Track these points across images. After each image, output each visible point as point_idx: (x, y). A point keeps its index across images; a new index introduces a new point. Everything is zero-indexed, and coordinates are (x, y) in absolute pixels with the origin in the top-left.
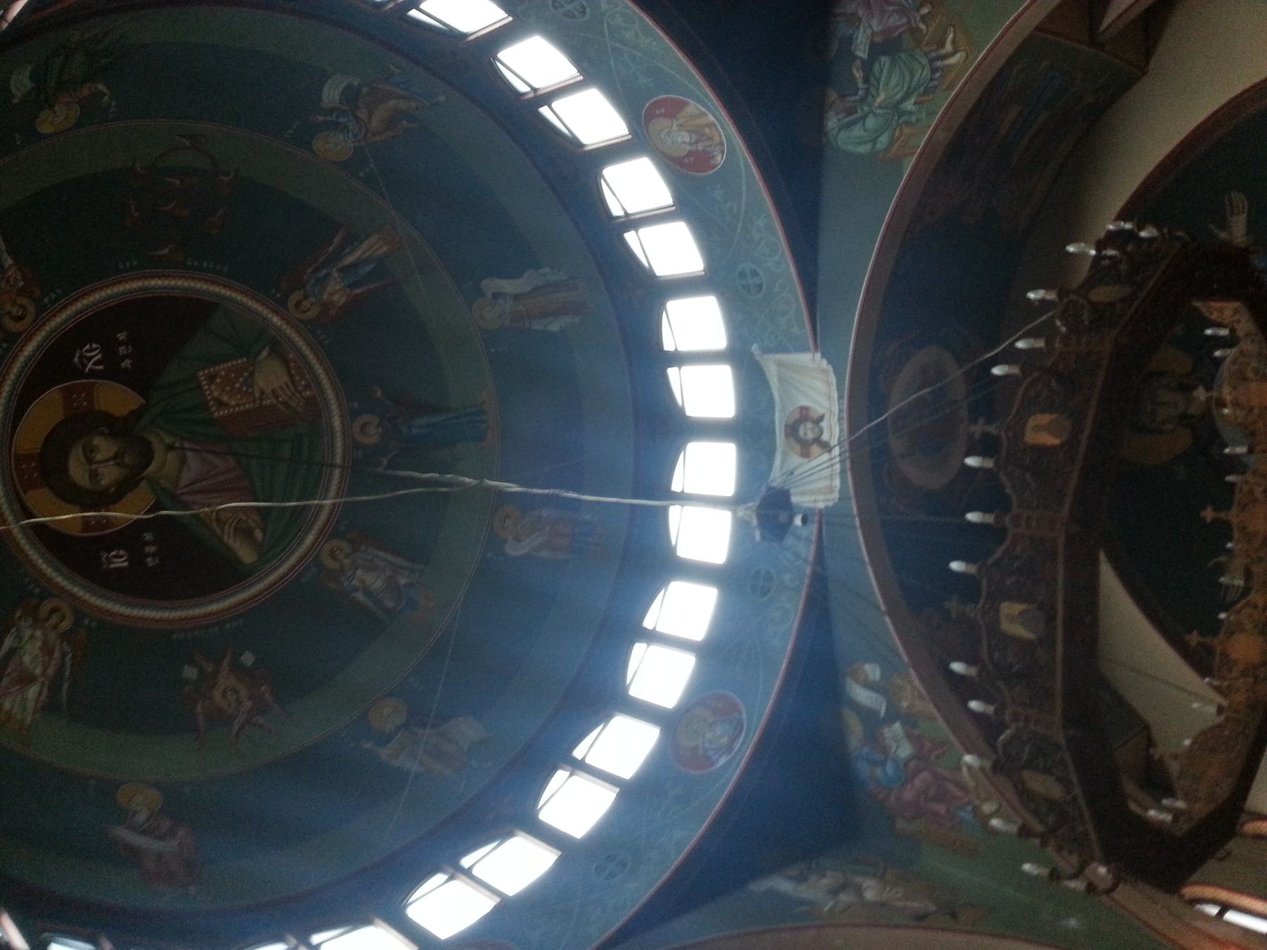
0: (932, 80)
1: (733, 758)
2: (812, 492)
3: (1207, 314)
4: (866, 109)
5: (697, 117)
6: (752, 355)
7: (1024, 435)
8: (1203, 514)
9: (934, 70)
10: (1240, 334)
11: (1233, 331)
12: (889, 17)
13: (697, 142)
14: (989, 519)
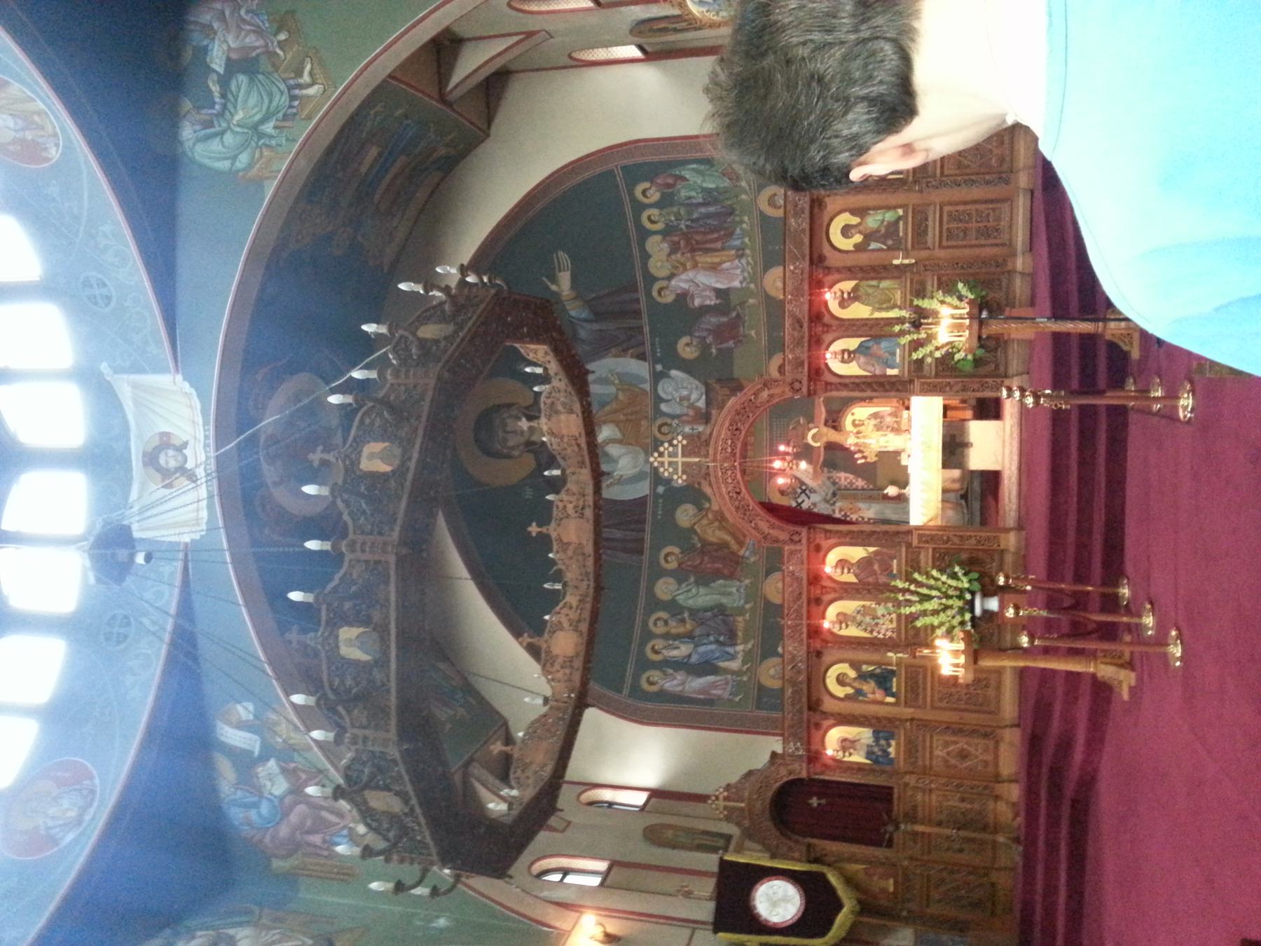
0: (291, 107)
1: (82, 834)
2: (175, 525)
3: (525, 355)
4: (224, 125)
6: (101, 374)
7: (359, 464)
8: (530, 529)
9: (293, 98)
10: (551, 373)
11: (546, 369)
12: (246, 36)
13: (23, 129)
14: (327, 546)
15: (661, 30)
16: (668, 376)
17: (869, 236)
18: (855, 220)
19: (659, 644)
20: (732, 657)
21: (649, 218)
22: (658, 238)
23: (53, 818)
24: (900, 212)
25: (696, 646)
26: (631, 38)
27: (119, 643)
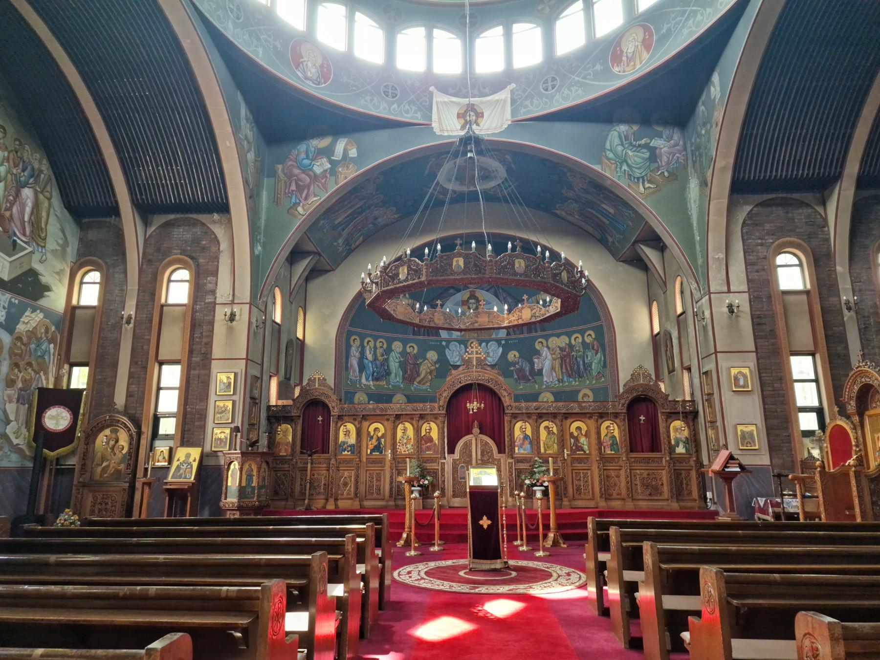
0: (634, 178)
4: (627, 146)
5: (640, 58)
6: (510, 84)
9: (638, 179)
13: (627, 56)
15: (666, 343)
16: (499, 347)
17: (577, 439)
18: (583, 433)
19: (372, 344)
20: (367, 379)
21: (577, 337)
22: (567, 342)
23: (307, 65)
24: (587, 452)
25: (372, 362)
26: (663, 331)
27: (384, 92)
